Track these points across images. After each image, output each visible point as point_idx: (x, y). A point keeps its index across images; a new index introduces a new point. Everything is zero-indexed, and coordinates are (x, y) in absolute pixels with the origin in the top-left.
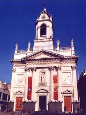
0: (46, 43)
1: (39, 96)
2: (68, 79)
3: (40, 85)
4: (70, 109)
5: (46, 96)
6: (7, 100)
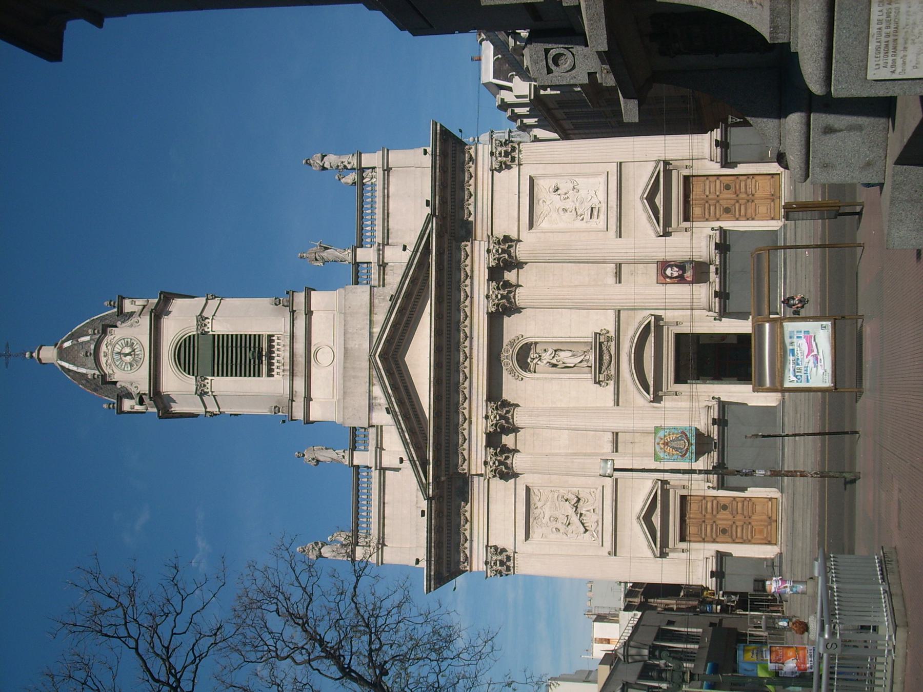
3: (602, 377)
4: (763, 183)
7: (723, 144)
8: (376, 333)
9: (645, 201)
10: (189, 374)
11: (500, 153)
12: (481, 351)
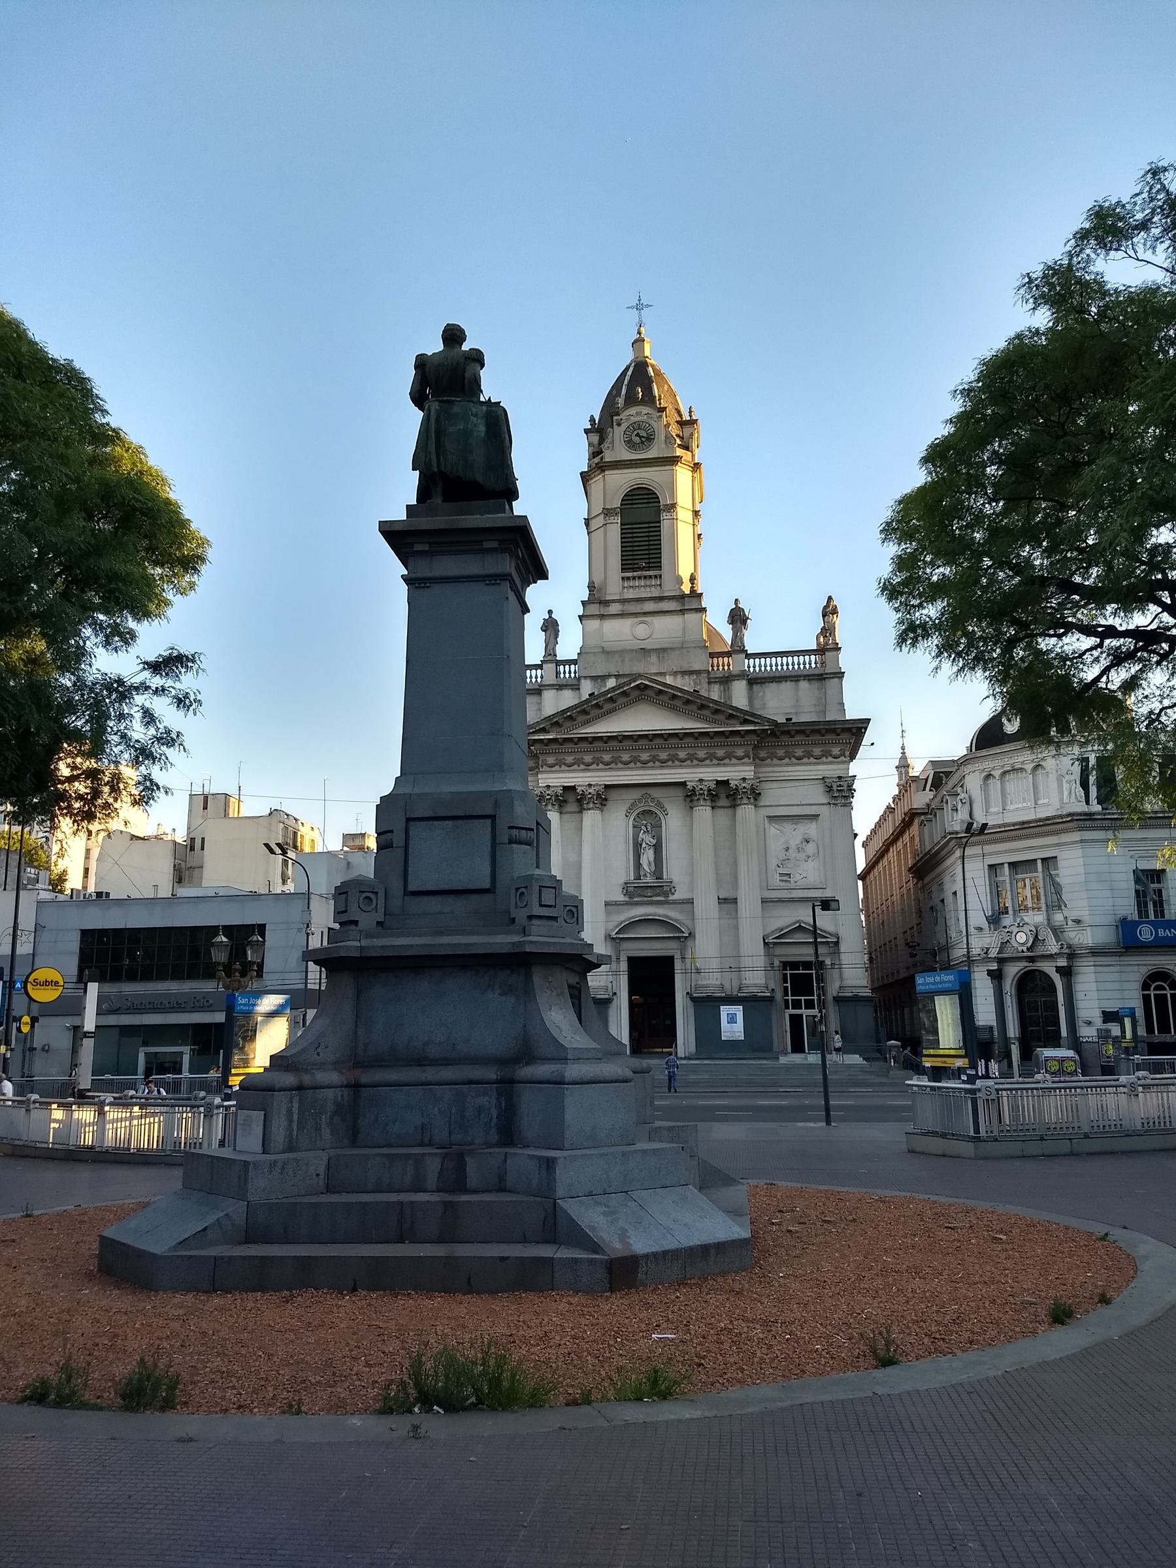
0: (658, 621)
1: (632, 961)
2: (802, 855)
5: (669, 961)
6: (1171, 994)
7: (856, 999)
8: (666, 680)
9: (797, 925)
10: (622, 500)
11: (840, 786)
12: (651, 777)
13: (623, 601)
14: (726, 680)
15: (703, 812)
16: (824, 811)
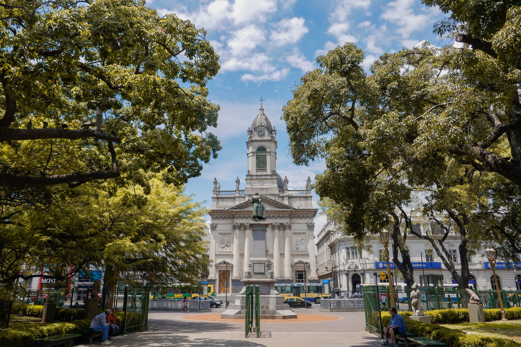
13: (257, 175)
14: (283, 197)
15: (277, 231)
16: (307, 232)
